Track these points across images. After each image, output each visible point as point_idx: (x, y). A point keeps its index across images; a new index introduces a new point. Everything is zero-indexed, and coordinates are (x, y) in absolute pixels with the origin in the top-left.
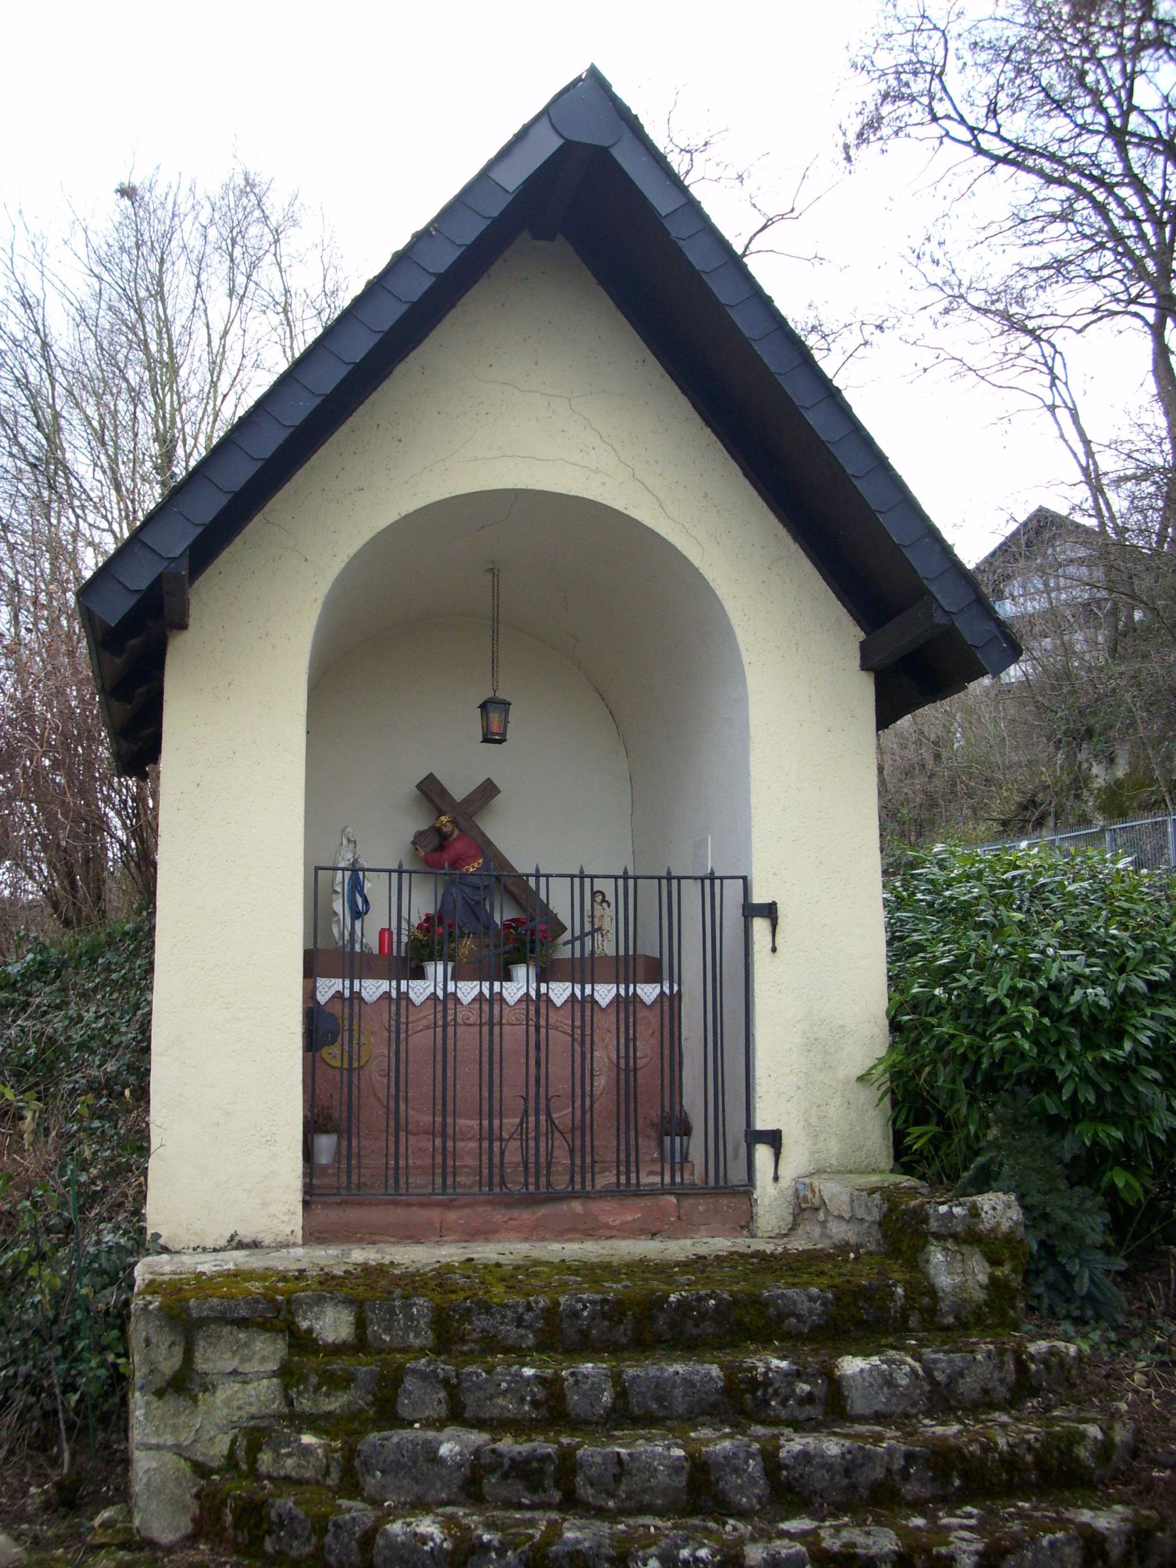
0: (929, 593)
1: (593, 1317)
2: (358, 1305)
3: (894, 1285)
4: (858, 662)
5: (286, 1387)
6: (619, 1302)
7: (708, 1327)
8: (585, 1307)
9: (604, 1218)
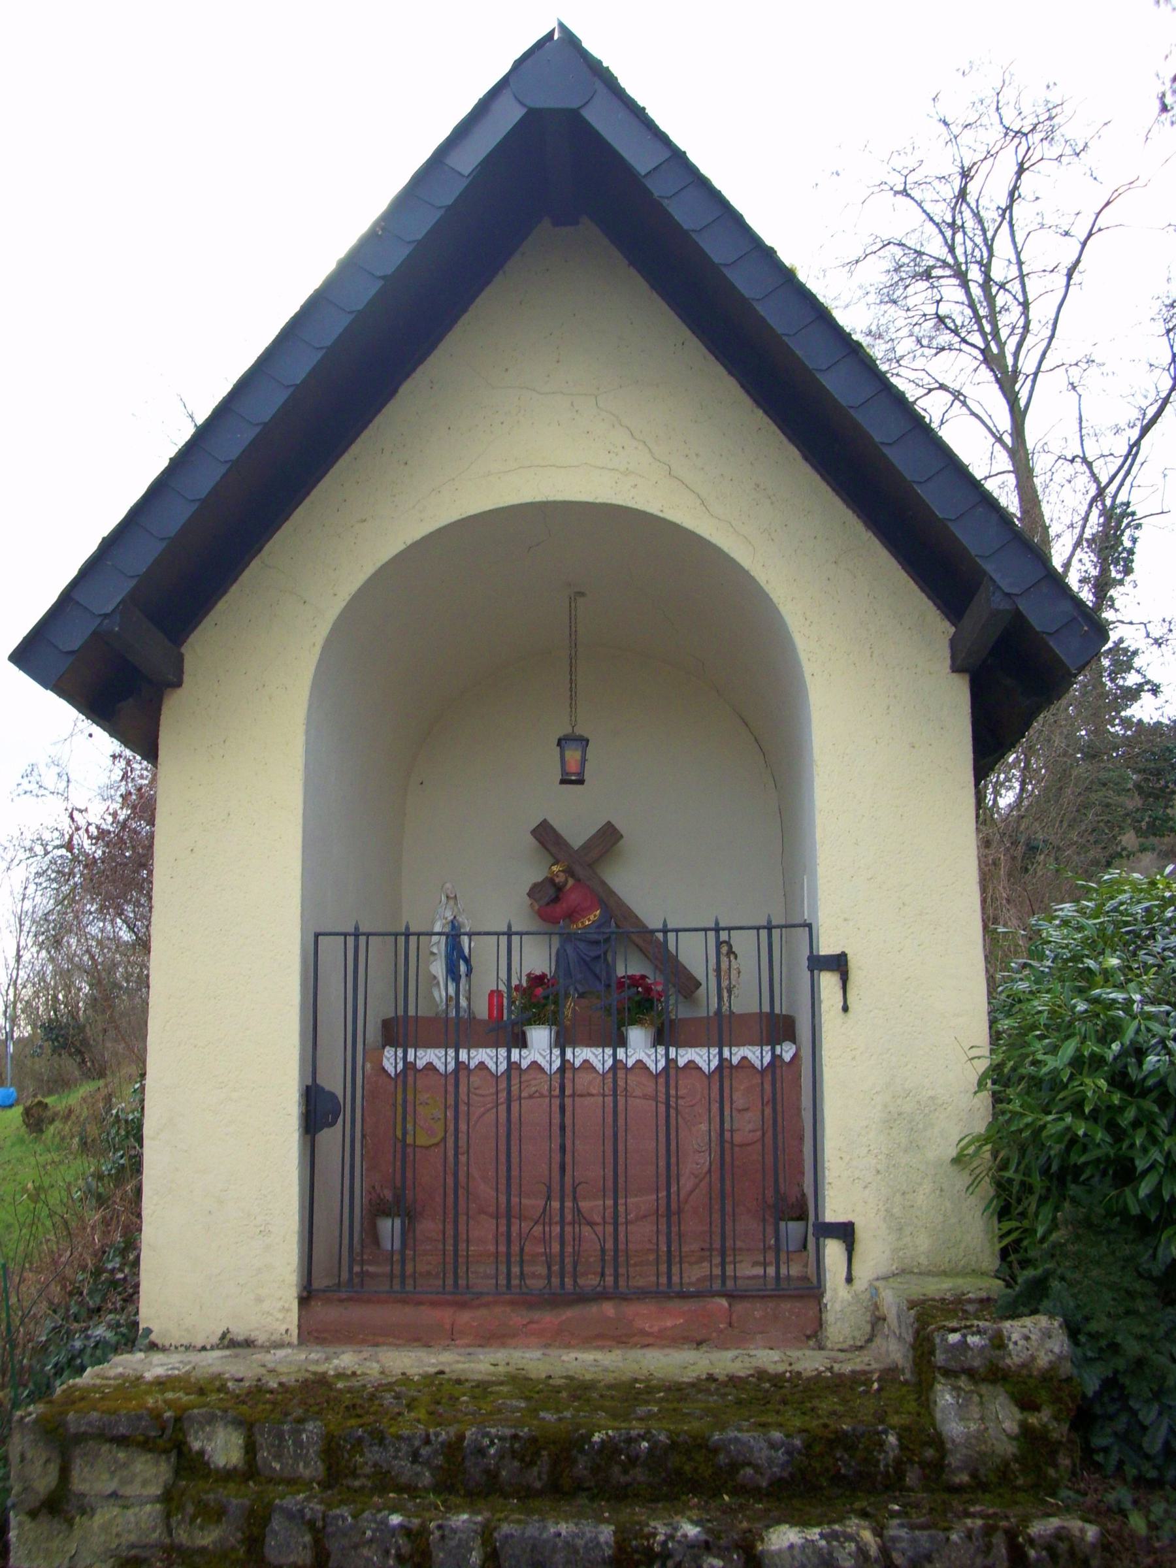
0: (985, 573)
1: (501, 1455)
2: (248, 1427)
3: (885, 1432)
4: (948, 662)
5: (168, 1516)
6: (534, 1440)
7: (639, 1474)
8: (492, 1443)
9: (639, 1324)
